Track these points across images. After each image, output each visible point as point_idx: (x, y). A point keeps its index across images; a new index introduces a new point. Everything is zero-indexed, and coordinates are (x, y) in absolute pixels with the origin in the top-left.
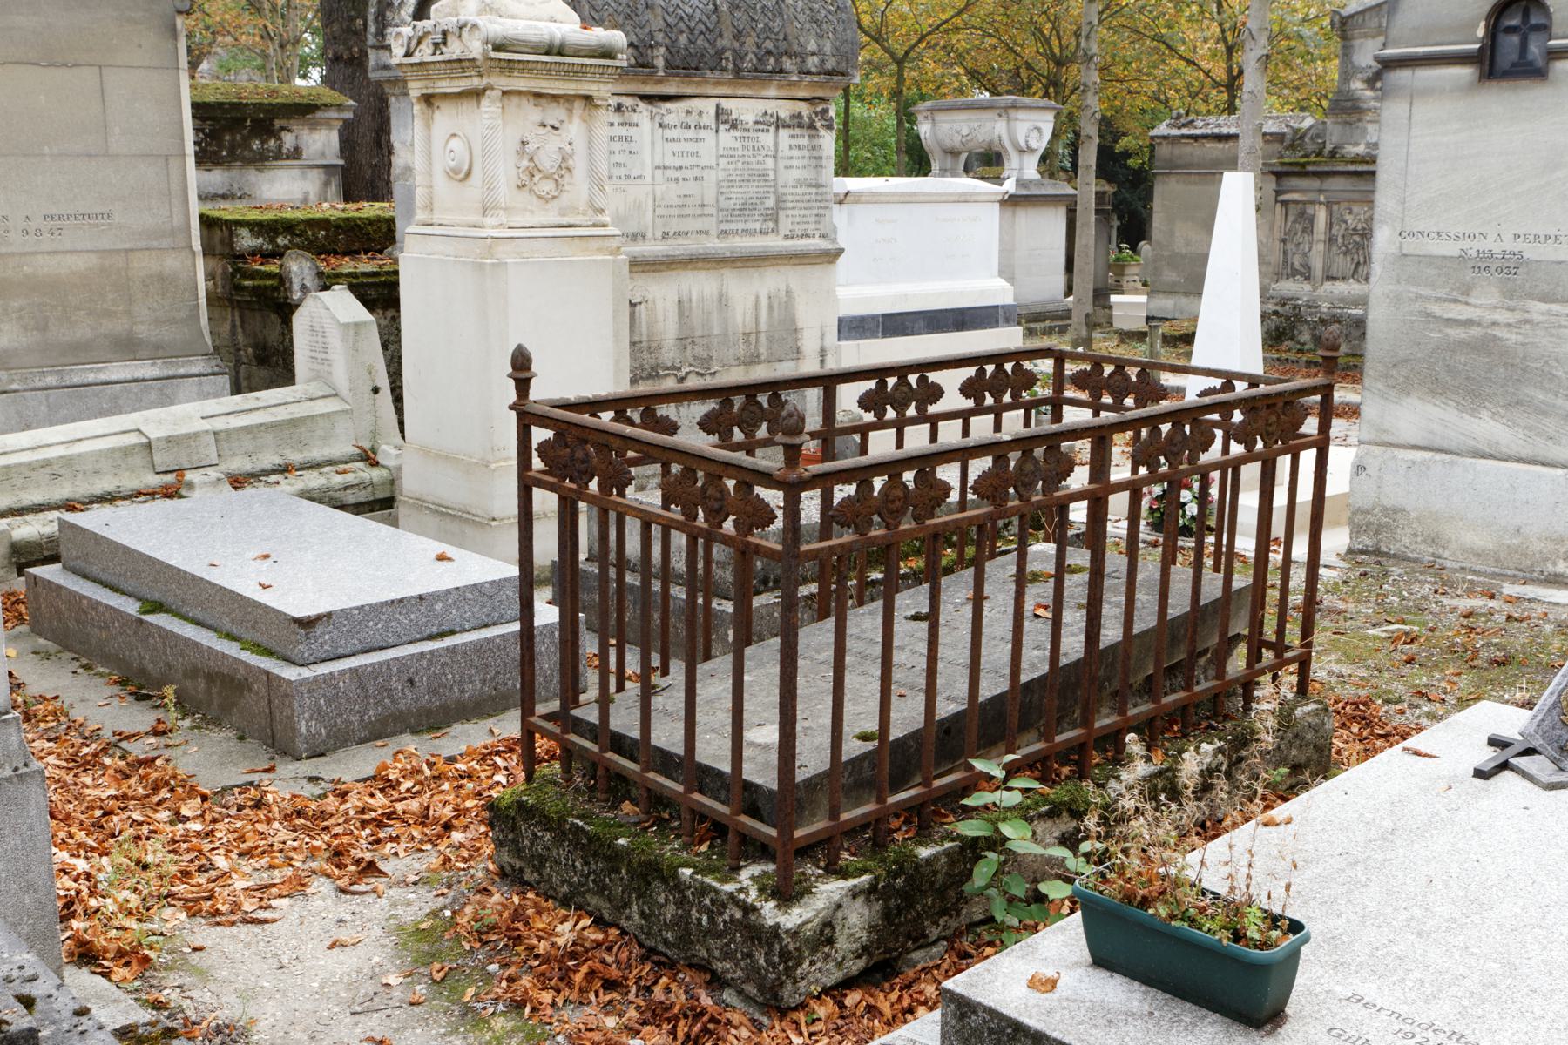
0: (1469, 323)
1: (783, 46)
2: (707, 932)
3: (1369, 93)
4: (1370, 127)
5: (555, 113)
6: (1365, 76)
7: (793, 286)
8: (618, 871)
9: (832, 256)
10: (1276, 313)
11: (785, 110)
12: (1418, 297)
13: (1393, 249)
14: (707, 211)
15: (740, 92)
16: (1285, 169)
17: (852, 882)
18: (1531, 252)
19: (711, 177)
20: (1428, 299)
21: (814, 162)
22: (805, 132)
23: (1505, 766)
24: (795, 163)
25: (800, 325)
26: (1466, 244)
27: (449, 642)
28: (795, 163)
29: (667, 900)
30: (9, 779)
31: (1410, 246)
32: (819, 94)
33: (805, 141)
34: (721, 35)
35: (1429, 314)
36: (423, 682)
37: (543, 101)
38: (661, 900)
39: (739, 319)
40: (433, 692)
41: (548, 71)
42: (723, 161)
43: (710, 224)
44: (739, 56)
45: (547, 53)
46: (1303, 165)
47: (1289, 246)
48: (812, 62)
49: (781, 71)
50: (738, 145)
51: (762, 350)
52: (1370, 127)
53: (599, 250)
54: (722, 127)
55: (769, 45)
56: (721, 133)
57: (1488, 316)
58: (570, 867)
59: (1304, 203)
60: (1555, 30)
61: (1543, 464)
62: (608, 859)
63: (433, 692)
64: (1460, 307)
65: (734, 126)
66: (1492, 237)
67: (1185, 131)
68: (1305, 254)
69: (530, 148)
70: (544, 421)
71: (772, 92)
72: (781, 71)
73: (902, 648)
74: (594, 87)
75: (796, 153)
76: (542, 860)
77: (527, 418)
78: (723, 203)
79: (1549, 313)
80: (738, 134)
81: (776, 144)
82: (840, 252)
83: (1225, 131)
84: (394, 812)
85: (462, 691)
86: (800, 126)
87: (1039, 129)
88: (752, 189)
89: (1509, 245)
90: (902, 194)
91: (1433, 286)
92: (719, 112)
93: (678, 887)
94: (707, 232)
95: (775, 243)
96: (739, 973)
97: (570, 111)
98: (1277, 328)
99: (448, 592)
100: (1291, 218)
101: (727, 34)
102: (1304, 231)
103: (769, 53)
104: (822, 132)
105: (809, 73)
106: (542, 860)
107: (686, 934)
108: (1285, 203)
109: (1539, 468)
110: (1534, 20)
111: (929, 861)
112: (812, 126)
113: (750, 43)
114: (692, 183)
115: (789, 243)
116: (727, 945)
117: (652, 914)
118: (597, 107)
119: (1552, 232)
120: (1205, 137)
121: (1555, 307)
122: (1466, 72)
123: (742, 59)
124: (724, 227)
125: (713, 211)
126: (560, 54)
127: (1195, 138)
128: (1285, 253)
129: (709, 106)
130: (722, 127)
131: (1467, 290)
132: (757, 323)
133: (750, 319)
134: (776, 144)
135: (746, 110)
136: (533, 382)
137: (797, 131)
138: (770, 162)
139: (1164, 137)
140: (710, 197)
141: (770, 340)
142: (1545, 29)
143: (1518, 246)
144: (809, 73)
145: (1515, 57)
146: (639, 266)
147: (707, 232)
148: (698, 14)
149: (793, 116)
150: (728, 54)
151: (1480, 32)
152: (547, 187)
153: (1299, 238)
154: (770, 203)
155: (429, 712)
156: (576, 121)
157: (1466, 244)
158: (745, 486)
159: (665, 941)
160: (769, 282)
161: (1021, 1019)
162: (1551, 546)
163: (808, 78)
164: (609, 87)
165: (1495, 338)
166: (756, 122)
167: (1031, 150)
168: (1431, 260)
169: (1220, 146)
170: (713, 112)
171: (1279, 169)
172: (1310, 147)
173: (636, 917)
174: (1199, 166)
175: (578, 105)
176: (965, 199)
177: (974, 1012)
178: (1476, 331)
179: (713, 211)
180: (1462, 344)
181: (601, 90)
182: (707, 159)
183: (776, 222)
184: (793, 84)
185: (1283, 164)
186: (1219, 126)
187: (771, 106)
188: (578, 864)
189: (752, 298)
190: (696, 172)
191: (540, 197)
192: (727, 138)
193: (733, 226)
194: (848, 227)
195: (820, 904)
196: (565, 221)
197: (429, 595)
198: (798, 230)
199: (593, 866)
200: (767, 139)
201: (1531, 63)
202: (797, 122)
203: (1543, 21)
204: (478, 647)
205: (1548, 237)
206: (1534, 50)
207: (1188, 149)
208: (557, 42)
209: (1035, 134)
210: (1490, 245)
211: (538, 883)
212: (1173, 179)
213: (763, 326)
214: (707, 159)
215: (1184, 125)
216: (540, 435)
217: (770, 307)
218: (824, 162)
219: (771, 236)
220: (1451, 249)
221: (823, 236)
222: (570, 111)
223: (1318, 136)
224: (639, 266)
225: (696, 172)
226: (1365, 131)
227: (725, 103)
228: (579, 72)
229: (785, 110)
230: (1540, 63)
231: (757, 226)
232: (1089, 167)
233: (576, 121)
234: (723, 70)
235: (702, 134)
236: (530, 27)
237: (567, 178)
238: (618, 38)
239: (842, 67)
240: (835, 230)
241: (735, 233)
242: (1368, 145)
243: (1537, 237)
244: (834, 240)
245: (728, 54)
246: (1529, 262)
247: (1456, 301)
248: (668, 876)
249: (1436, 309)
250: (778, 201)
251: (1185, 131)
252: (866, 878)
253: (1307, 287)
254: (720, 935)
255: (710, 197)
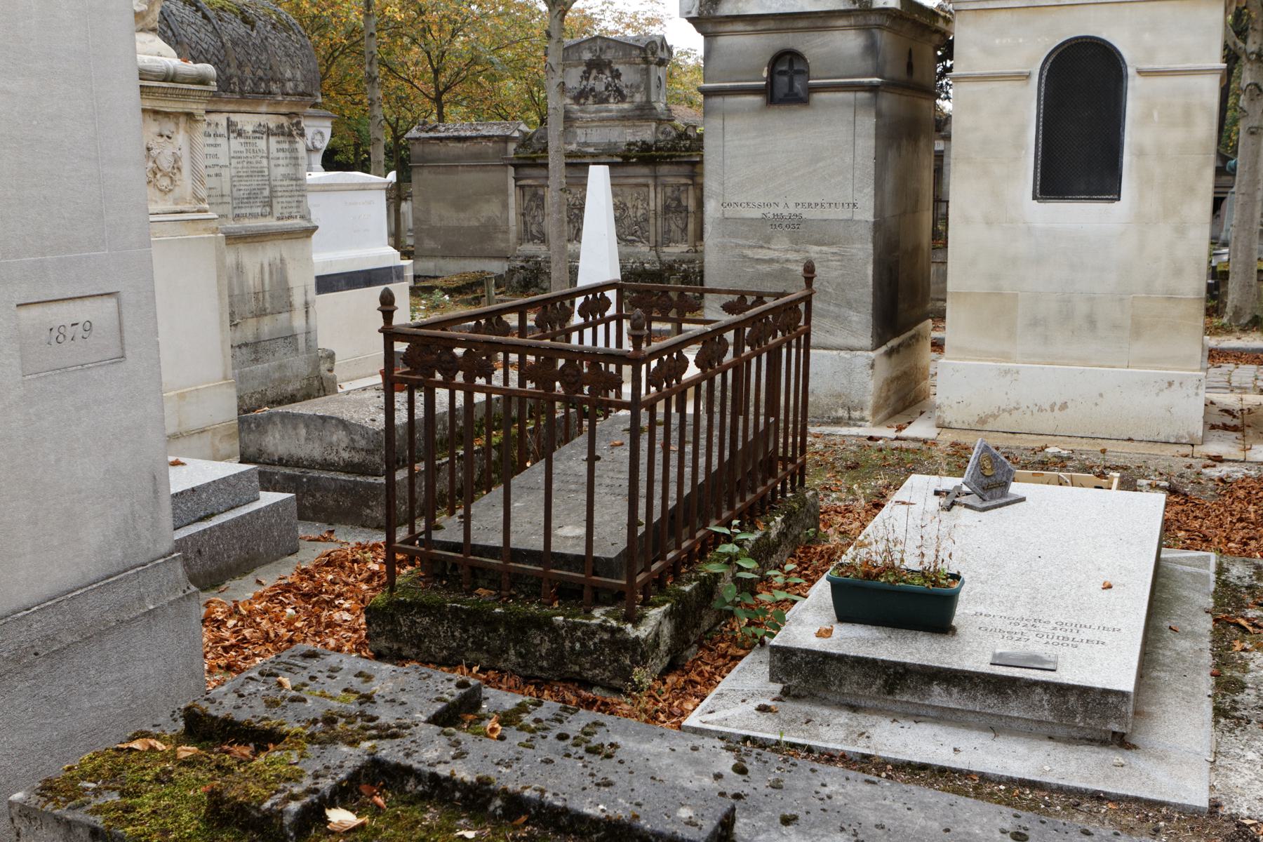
0: (771, 261)
1: (270, 73)
2: (579, 654)
3: (576, 107)
4: (579, 131)
5: (168, 127)
6: (572, 94)
7: (285, 255)
8: (496, 630)
9: (309, 232)
10: (522, 267)
11: (272, 121)
12: (737, 245)
13: (719, 215)
14: (225, 199)
15: (243, 109)
16: (520, 162)
17: (663, 608)
18: (807, 214)
19: (226, 173)
20: (743, 246)
21: (293, 162)
22: (286, 139)
23: (953, 504)
24: (281, 162)
25: (291, 285)
26: (766, 210)
27: (216, 521)
28: (281, 162)
29: (542, 640)
30: (182, 598)
31: (730, 212)
32: (294, 110)
33: (286, 146)
34: (228, 65)
35: (745, 257)
36: (206, 551)
37: (159, 117)
38: (537, 641)
39: (251, 283)
40: (212, 559)
41: (166, 94)
42: (234, 161)
43: (227, 209)
44: (242, 82)
45: (164, 81)
46: (534, 159)
47: (528, 218)
48: (289, 86)
49: (270, 93)
50: (243, 149)
51: (267, 305)
52: (579, 131)
53: (205, 230)
54: (232, 135)
55: (260, 73)
56: (232, 141)
57: (783, 256)
58: (448, 635)
59: (536, 186)
60: (812, 74)
61: (824, 348)
62: (486, 623)
63: (212, 559)
64: (765, 251)
65: (240, 134)
66: (782, 205)
67: (432, 134)
68: (539, 224)
69: (154, 153)
70: (402, 337)
71: (263, 109)
72: (270, 93)
73: (601, 476)
74: (194, 106)
75: (281, 155)
76: (420, 638)
77: (390, 335)
78: (236, 194)
79: (821, 252)
80: (242, 140)
81: (268, 148)
82: (316, 228)
83: (462, 134)
84: (245, 638)
85: (229, 557)
86: (283, 134)
87: (321, 133)
88: (254, 183)
89: (793, 210)
90: (324, 185)
91: (747, 238)
92: (230, 125)
93: (554, 629)
94: (226, 216)
95: (271, 223)
96: (607, 674)
97: (177, 124)
98: (525, 279)
99: (209, 484)
100: (527, 198)
101: (234, 64)
102: (537, 207)
103: (261, 79)
104: (298, 139)
105: (288, 94)
106: (420, 638)
107: (558, 658)
108: (522, 187)
109: (822, 351)
110: (796, 68)
111: (690, 593)
112: (290, 135)
113: (247, 70)
114: (214, 178)
115: (281, 223)
116: (598, 658)
117: (528, 652)
118: (197, 121)
119: (819, 201)
120: (448, 138)
121: (824, 248)
122: (757, 100)
123: (244, 83)
124: (237, 211)
125: (228, 199)
126: (172, 81)
127: (440, 139)
128: (525, 223)
129: (222, 119)
130: (232, 135)
131: (768, 240)
132: (263, 284)
133: (258, 281)
134: (268, 148)
135: (247, 122)
136: (395, 313)
137: (281, 138)
138: (265, 162)
139: (417, 139)
140: (227, 190)
141: (272, 297)
142: (805, 73)
143: (799, 210)
144: (288, 94)
145: (786, 90)
146: (234, 239)
147: (226, 216)
148: (211, 49)
149: (278, 127)
150: (235, 79)
151: (765, 74)
152: (165, 182)
153: (534, 212)
154: (266, 193)
155: (211, 575)
156: (182, 132)
157: (766, 210)
158: (594, 365)
159: (541, 669)
160: (268, 253)
161: (828, 650)
162: (834, 400)
163: (288, 98)
164: (204, 106)
165: (789, 270)
166: (254, 132)
167: (316, 150)
168: (744, 221)
169: (460, 145)
170: (225, 124)
171: (516, 162)
172: (537, 146)
173: (513, 658)
174: (445, 161)
175: (182, 119)
176: (363, 188)
177: (795, 655)
178: (776, 266)
179: (228, 199)
180: (768, 275)
181: (198, 108)
182: (223, 160)
183: (271, 207)
184: (278, 103)
185: (519, 158)
186: (457, 130)
187: (263, 119)
188: (457, 634)
189: (258, 266)
190: (217, 170)
191: (161, 190)
192: (236, 144)
193: (243, 211)
194: (320, 210)
195: (653, 623)
196: (179, 208)
197: (198, 487)
198: (286, 212)
199: (472, 632)
200: (262, 144)
201: (796, 94)
202: (280, 132)
203: (802, 68)
204: (237, 522)
205: (816, 205)
206: (798, 86)
207: (436, 148)
208: (172, 71)
209: (318, 137)
210: (780, 210)
211: (417, 654)
212: (425, 171)
213: (267, 287)
214: (223, 160)
215: (431, 130)
216: (400, 347)
217: (271, 273)
218: (300, 161)
219: (269, 218)
220: (756, 213)
221: (302, 217)
222: (177, 124)
223: (542, 138)
224: (234, 239)
225: (217, 170)
226: (575, 134)
227: (234, 117)
228: (185, 95)
229: (272, 121)
230: (802, 94)
231: (259, 210)
232: (379, 162)
233: (182, 132)
234: (232, 92)
235: (219, 140)
236: (152, 61)
237: (178, 176)
238: (208, 69)
239: (309, 90)
240: (309, 213)
241: (244, 216)
242: (578, 144)
243: (810, 205)
244: (309, 220)
245: (235, 79)
246: (806, 221)
247: (762, 247)
248: (544, 624)
249: (749, 253)
250: (271, 192)
251: (432, 134)
252: (668, 605)
253: (544, 248)
254: (591, 653)
255: (227, 190)
